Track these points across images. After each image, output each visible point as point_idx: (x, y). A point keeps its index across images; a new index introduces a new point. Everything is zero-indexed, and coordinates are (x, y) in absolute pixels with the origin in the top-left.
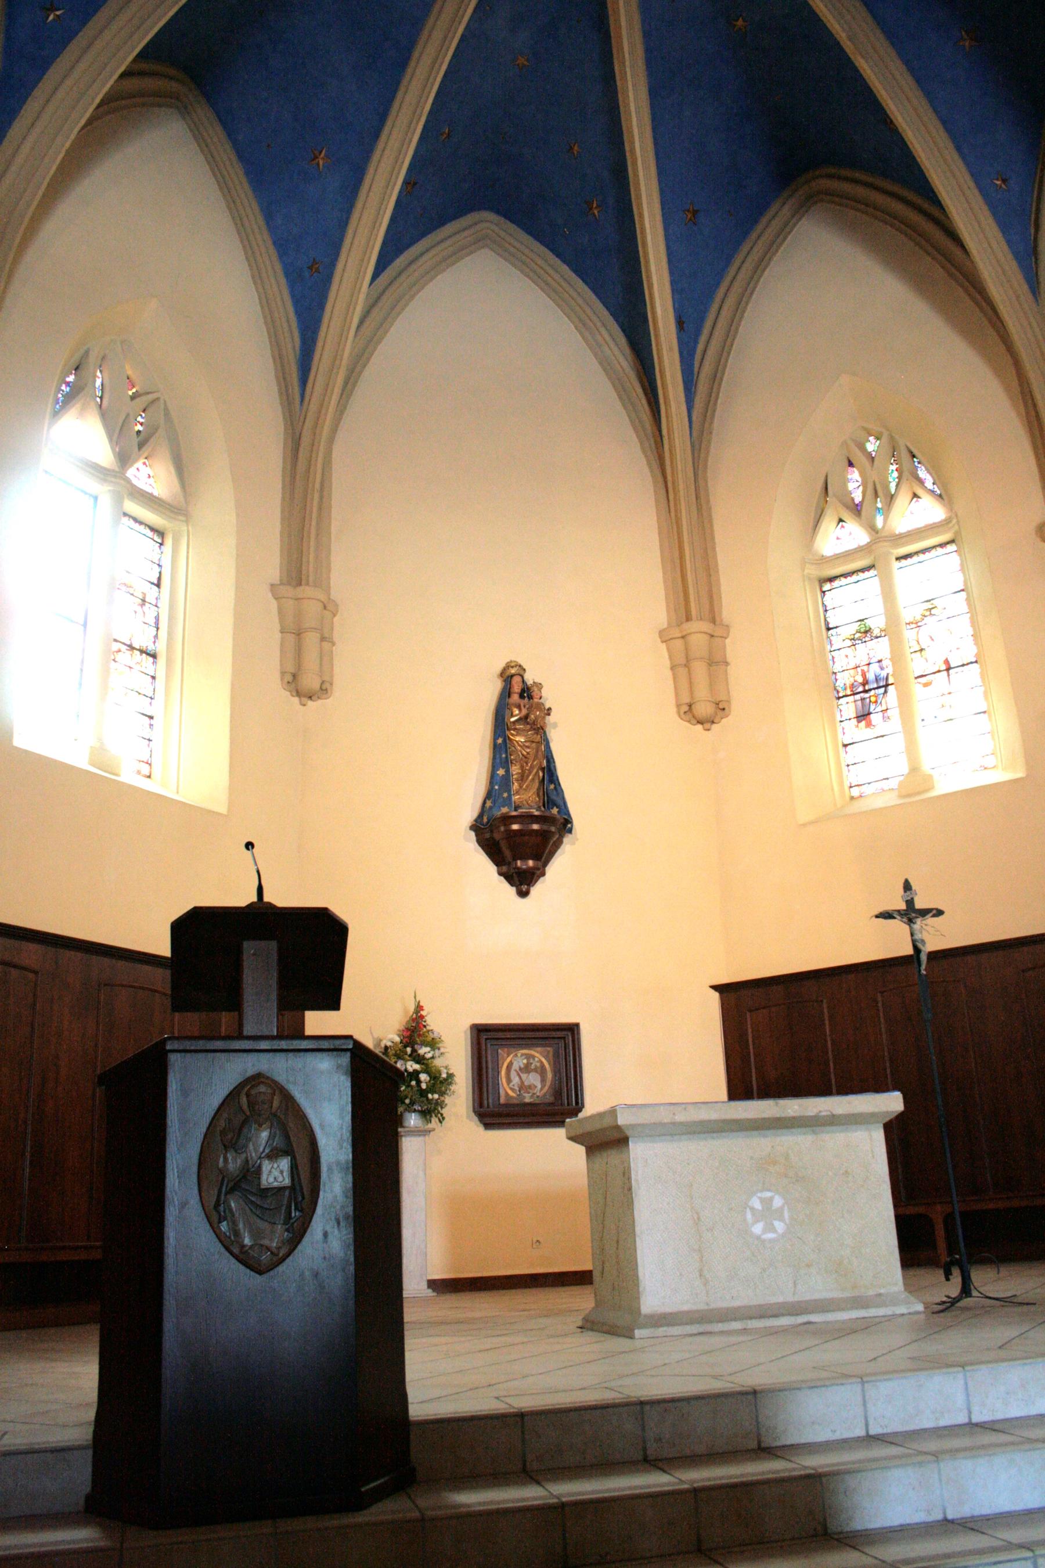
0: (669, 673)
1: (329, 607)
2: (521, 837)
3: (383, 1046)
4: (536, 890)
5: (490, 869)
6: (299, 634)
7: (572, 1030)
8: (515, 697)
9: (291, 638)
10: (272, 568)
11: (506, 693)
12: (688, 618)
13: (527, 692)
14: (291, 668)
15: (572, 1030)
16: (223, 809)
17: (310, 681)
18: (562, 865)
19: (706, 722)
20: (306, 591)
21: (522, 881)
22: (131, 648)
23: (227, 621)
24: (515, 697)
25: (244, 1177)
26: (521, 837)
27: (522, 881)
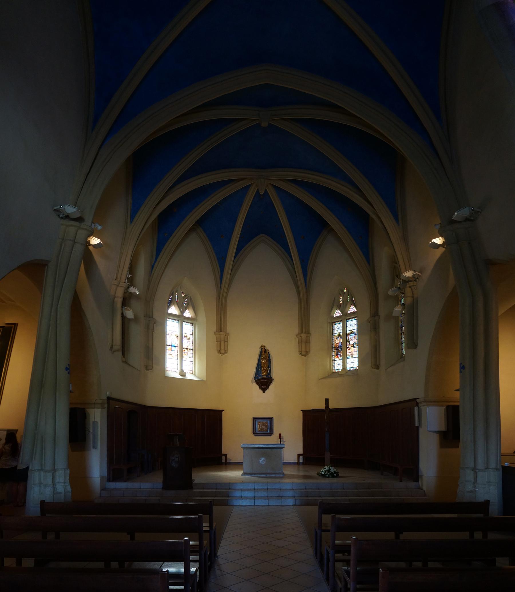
0: (298, 344)
1: (227, 334)
2: (264, 381)
3: (105, 398)
4: (266, 391)
5: (257, 387)
6: (220, 341)
7: (254, 418)
8: (263, 353)
9: (219, 343)
10: (214, 329)
11: (261, 351)
12: (302, 333)
13: (266, 351)
14: (219, 349)
15: (254, 418)
16: (205, 380)
17: (223, 352)
18: (271, 387)
19: (305, 355)
20: (221, 333)
21: (264, 390)
22: (187, 349)
23: (205, 342)
24: (263, 353)
25: (126, 362)
26: (264, 381)
27: (264, 390)
